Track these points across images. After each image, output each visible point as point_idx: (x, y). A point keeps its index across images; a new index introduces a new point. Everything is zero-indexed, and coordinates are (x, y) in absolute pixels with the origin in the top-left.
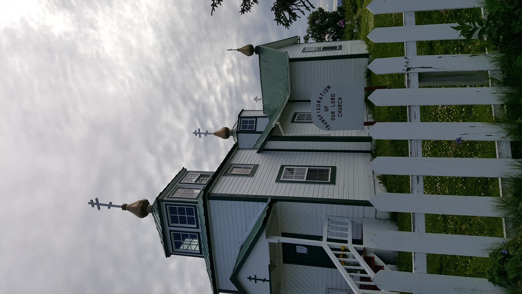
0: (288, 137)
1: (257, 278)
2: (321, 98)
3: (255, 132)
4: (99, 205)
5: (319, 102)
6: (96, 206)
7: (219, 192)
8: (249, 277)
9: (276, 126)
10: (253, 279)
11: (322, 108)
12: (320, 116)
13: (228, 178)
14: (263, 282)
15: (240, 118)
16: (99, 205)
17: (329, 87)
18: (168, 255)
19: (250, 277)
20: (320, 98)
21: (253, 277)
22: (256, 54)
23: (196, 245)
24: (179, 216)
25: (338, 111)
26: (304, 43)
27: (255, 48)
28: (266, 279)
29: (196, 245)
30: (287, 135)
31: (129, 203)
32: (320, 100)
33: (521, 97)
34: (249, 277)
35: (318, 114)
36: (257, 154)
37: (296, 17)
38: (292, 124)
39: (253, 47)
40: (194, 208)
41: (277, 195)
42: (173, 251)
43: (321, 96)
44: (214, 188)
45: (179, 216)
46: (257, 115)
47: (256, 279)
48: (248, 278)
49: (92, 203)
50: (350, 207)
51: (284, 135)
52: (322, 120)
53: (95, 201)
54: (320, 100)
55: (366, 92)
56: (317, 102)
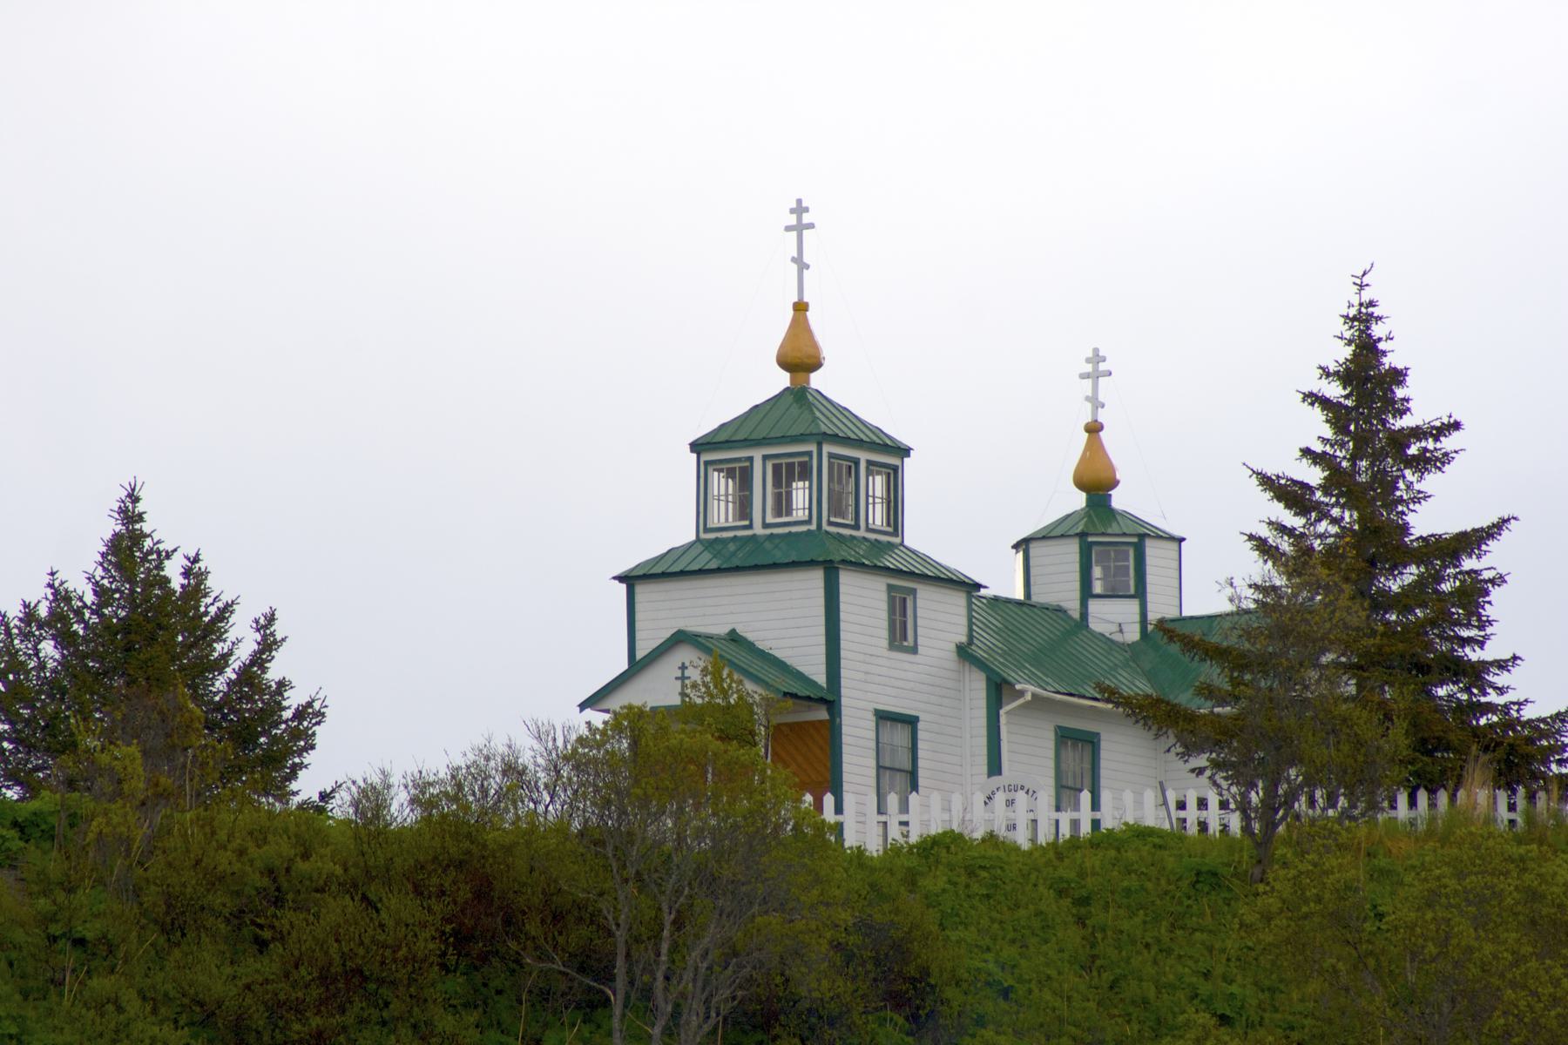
0: (999, 721)
1: (805, 232)
3: (1086, 593)
4: (1095, 376)
6: (793, 220)
7: (841, 580)
8: (804, 205)
9: (1021, 693)
10: (683, 673)
13: (1052, 744)
15: (1135, 540)
16: (1095, 376)
18: (697, 447)
19: (807, 210)
26: (1153, 616)
28: (1089, 393)
30: (1003, 720)
31: (812, 316)
33: (1, 924)
34: (804, 205)
36: (953, 647)
38: (1052, 735)
41: (845, 711)
42: (706, 463)
44: (1099, 801)
46: (1150, 597)
47: (800, 228)
49: (1097, 358)
51: (1002, 712)
53: (1102, 367)
55: (1352, 366)
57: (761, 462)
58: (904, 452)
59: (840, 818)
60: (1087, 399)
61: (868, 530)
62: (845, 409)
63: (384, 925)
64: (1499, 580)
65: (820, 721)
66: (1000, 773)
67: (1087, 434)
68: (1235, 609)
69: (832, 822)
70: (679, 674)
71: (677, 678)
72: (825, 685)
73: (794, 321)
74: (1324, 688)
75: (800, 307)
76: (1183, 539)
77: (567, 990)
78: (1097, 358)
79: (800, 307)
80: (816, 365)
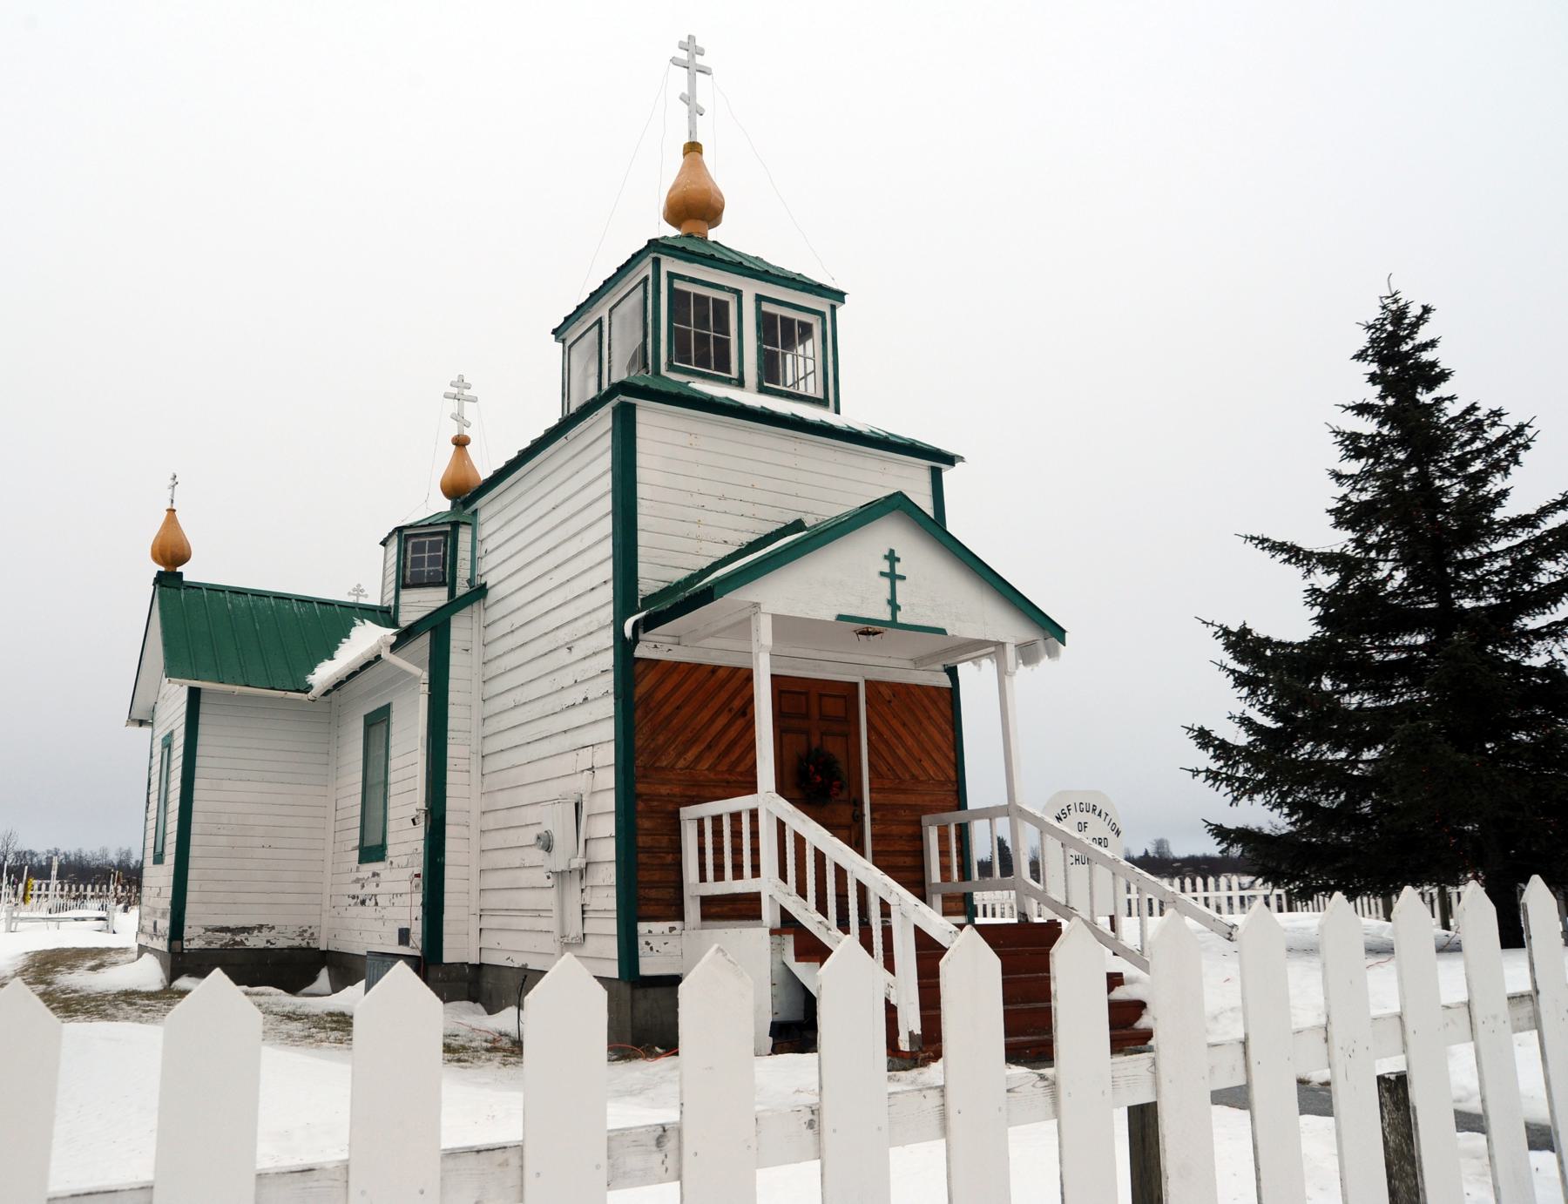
2: (1100, 815)
5: (1094, 810)
10: (892, 567)
11: (1084, 817)
12: (1069, 810)
14: (900, 610)
17: (1118, 833)
20: (1100, 812)
21: (899, 570)
22: (159, 572)
23: (805, 361)
24: (714, 336)
25: (1302, 911)
27: (179, 569)
29: (805, 361)
31: (708, 157)
32: (1097, 812)
35: (1072, 807)
37: (1240, 738)
39: (179, 566)
40: (623, 394)
43: (1103, 815)
45: (714, 336)
48: (892, 551)
49: (690, 46)
50: (198, 783)
52: (1062, 816)
54: (1097, 812)
56: (1094, 806)
57: (746, 377)
58: (839, 296)
59: (692, 910)
60: (886, 557)
61: (785, 385)
62: (757, 258)
63: (495, 1039)
64: (1361, 356)
65: (937, 689)
66: (759, 876)
67: (454, 446)
68: (676, 767)
69: (1446, 480)
70: (886, 567)
71: (882, 574)
72: (364, 981)
73: (168, 517)
74: (1401, 642)
75: (693, 148)
76: (950, 460)
77: (1394, 573)
78: (690, 46)
79: (693, 148)
80: (183, 558)
